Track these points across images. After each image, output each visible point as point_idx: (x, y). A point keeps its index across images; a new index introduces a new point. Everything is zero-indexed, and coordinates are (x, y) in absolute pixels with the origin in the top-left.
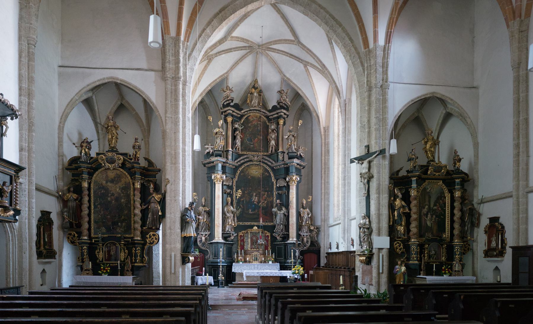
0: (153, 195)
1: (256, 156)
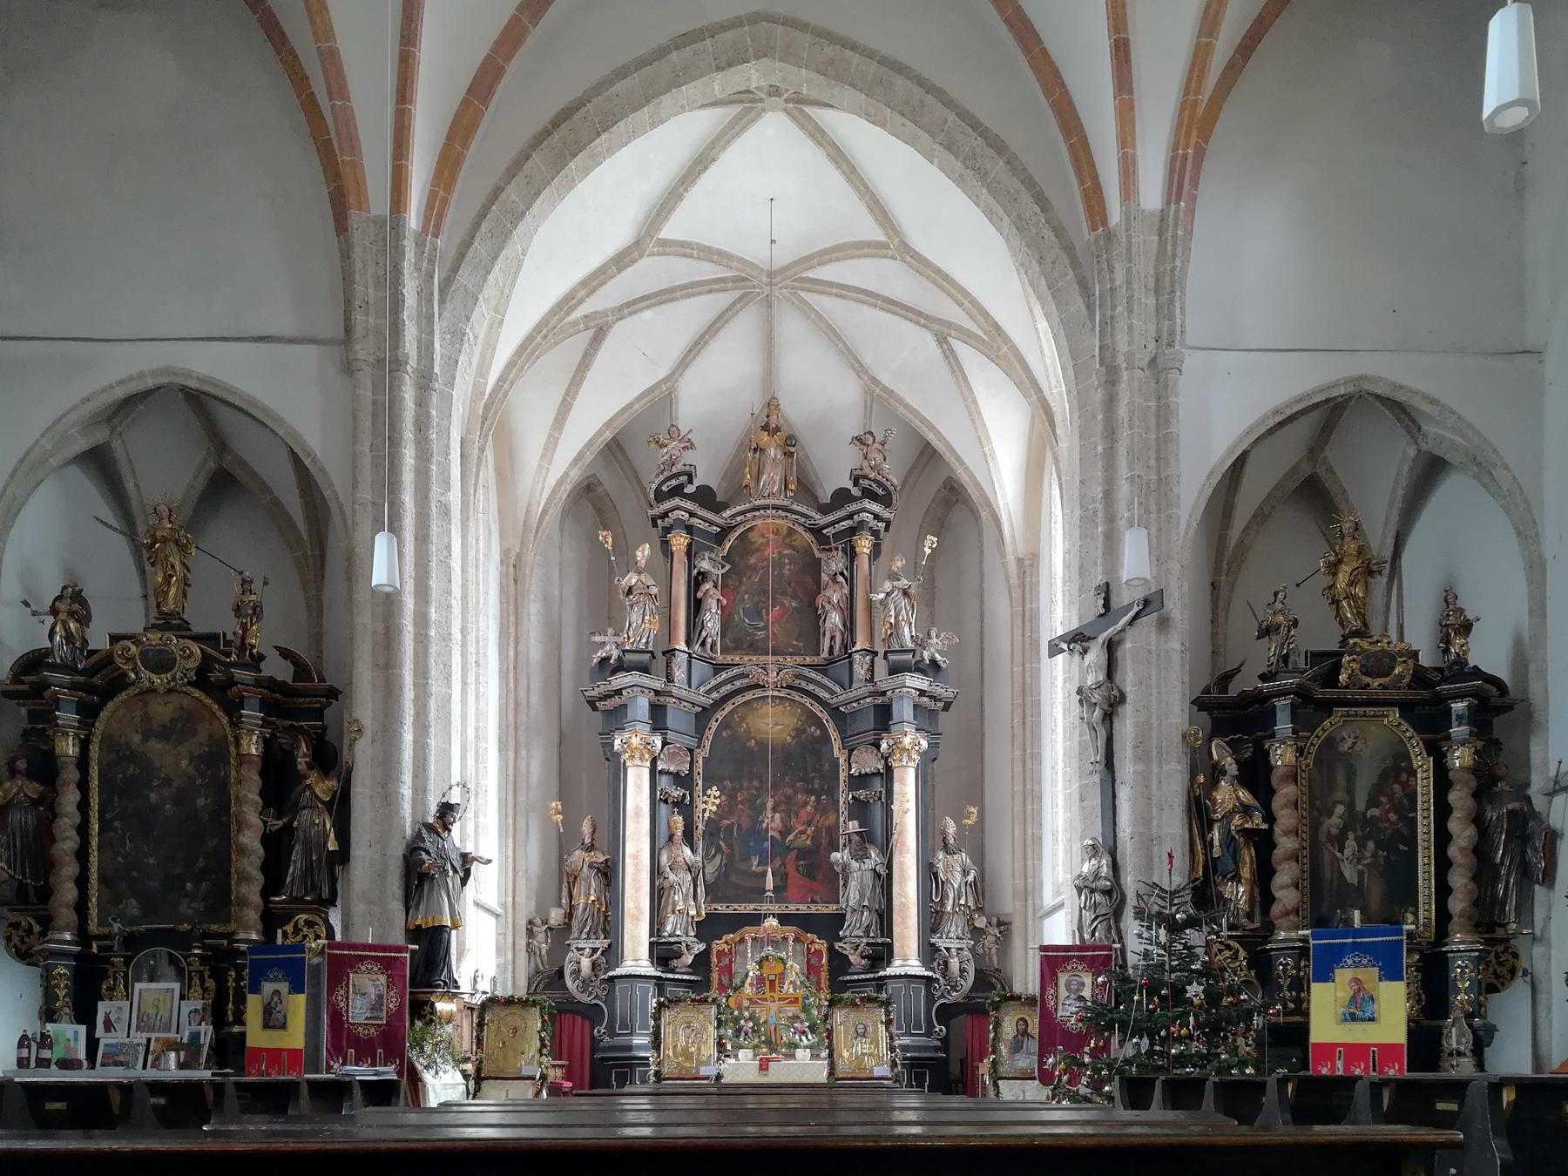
0: (308, 782)
1: (772, 671)
